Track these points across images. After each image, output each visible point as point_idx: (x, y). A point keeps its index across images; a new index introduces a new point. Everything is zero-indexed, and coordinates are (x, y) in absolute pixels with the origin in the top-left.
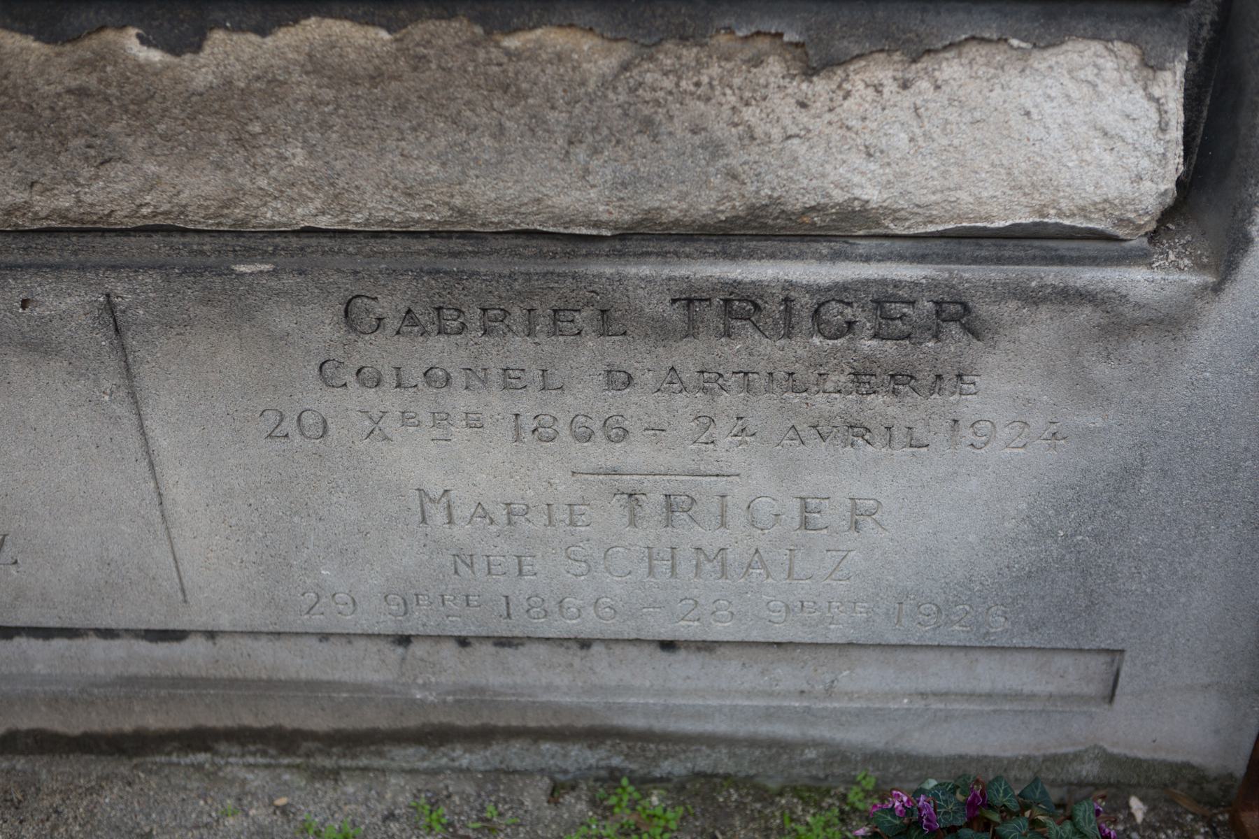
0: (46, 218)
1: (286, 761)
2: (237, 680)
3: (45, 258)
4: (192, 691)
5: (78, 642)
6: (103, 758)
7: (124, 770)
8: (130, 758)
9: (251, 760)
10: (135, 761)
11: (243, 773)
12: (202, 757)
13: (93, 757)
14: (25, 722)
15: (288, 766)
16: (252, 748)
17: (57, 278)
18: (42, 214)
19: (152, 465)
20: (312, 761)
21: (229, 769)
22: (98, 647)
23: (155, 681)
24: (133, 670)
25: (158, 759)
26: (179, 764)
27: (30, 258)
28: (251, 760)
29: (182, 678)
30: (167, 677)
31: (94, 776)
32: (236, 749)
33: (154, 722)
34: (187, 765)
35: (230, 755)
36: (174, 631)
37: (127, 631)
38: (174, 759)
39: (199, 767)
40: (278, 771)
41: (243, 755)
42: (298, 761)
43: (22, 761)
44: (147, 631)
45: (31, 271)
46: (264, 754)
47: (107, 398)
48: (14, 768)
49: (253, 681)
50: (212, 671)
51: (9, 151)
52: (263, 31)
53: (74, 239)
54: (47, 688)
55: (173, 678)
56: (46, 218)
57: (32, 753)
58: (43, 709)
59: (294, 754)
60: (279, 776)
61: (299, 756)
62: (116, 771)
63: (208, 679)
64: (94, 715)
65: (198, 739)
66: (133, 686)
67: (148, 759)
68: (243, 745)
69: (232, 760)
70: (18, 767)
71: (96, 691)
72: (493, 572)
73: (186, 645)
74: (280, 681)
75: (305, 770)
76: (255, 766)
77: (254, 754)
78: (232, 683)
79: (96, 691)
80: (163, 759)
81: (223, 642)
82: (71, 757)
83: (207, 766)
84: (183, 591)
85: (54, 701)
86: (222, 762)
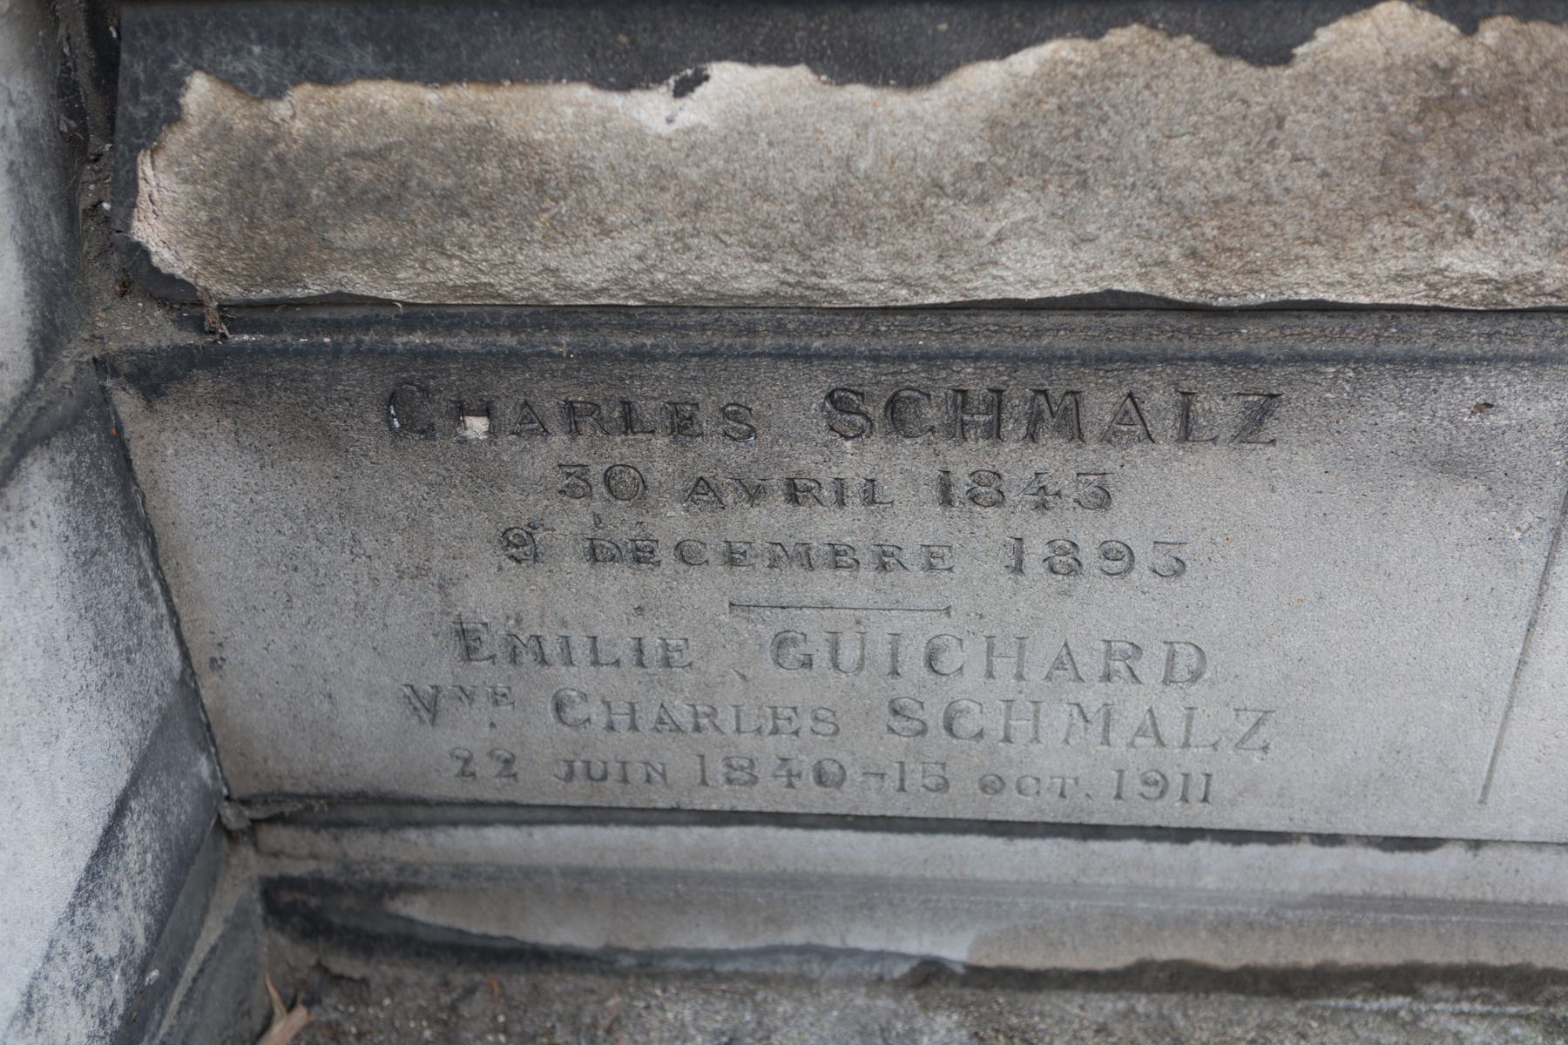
0: (1552, 295)
1: (1512, 1010)
2: (1483, 902)
3: (1513, 348)
4: (1426, 917)
5: (1283, 850)
6: (1256, 1000)
7: (1290, 1016)
8: (1296, 999)
9: (1465, 1006)
10: (1299, 1005)
11: (1454, 1025)
12: (1396, 1001)
13: (1242, 998)
14: (1166, 950)
15: (1518, 1016)
16: (1474, 991)
17: (1537, 375)
18: (1548, 289)
19: (1531, 625)
20: (1552, 1010)
21: (1432, 1018)
22: (1305, 857)
23: (1367, 902)
24: (1340, 887)
25: (1332, 1003)
26: (1361, 1010)
27: (1497, 346)
28: (1465, 1006)
29: (1406, 898)
30: (1385, 898)
31: (1252, 1023)
32: (1450, 993)
33: (1349, 954)
34: (1371, 1011)
35: (1438, 1000)
36: (1426, 839)
37: (1358, 837)
38: (1357, 1003)
39: (1391, 1015)
40: (1503, 1022)
41: (1458, 1000)
42: (1533, 1009)
43: (1144, 1000)
44: (1386, 839)
45: (1501, 365)
46: (1487, 999)
47: (1517, 535)
48: (1132, 1010)
49: (1506, 904)
50: (1453, 891)
51: (1546, 201)
52: (1095, 34)
53: (1558, 322)
54: (1221, 908)
55: (1393, 898)
56: (1552, 295)
57: (1158, 991)
58: (1203, 935)
59: (1533, 1002)
60: (1505, 1030)
61: (1536, 1004)
62: (1280, 1018)
63: (1442, 901)
64: (1270, 945)
65: (1405, 979)
66: (1336, 907)
67: (1320, 1002)
68: (1462, 987)
69: (1438, 1007)
70: (1140, 1008)
71: (1290, 914)
72: (603, 658)
73: (1434, 856)
74: (1545, 905)
75: (1536, 1022)
76: (1469, 1014)
77: (1472, 1000)
78: (1477, 906)
79: (1290, 914)
80: (1342, 1003)
81: (1487, 854)
82: (1212, 997)
83: (1402, 1013)
84: (1486, 788)
85: (1222, 926)
86: (1423, 1008)
